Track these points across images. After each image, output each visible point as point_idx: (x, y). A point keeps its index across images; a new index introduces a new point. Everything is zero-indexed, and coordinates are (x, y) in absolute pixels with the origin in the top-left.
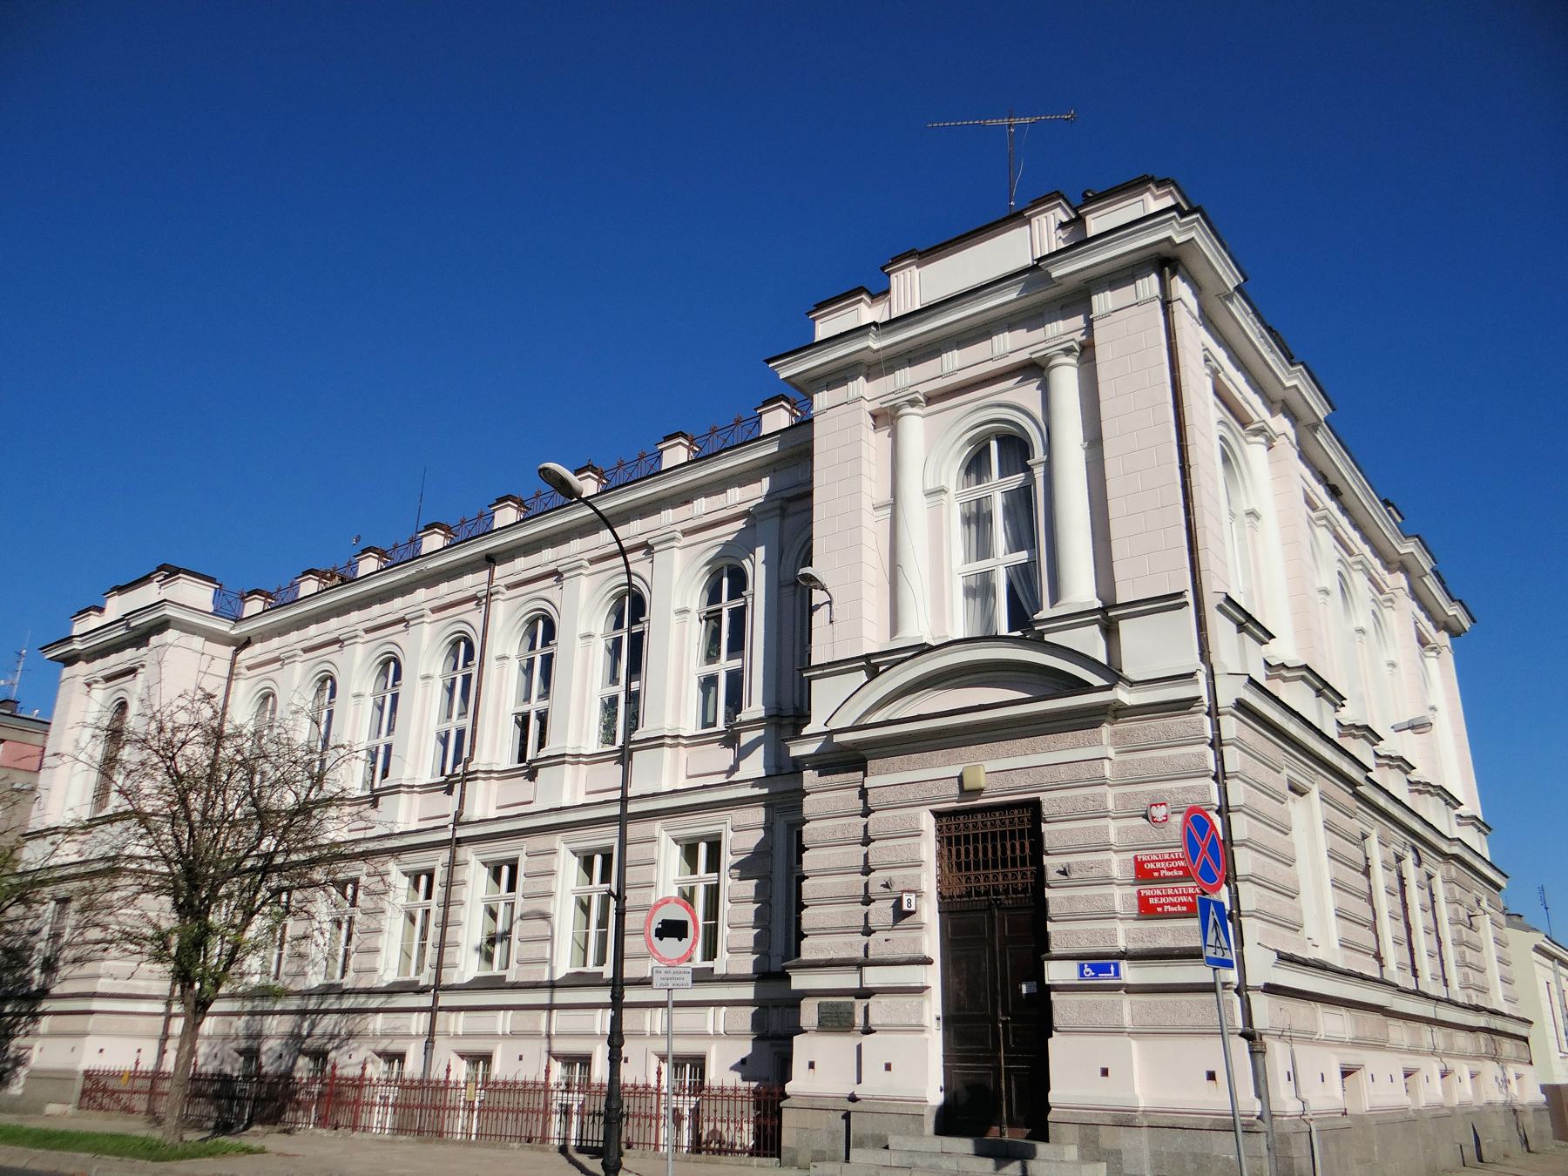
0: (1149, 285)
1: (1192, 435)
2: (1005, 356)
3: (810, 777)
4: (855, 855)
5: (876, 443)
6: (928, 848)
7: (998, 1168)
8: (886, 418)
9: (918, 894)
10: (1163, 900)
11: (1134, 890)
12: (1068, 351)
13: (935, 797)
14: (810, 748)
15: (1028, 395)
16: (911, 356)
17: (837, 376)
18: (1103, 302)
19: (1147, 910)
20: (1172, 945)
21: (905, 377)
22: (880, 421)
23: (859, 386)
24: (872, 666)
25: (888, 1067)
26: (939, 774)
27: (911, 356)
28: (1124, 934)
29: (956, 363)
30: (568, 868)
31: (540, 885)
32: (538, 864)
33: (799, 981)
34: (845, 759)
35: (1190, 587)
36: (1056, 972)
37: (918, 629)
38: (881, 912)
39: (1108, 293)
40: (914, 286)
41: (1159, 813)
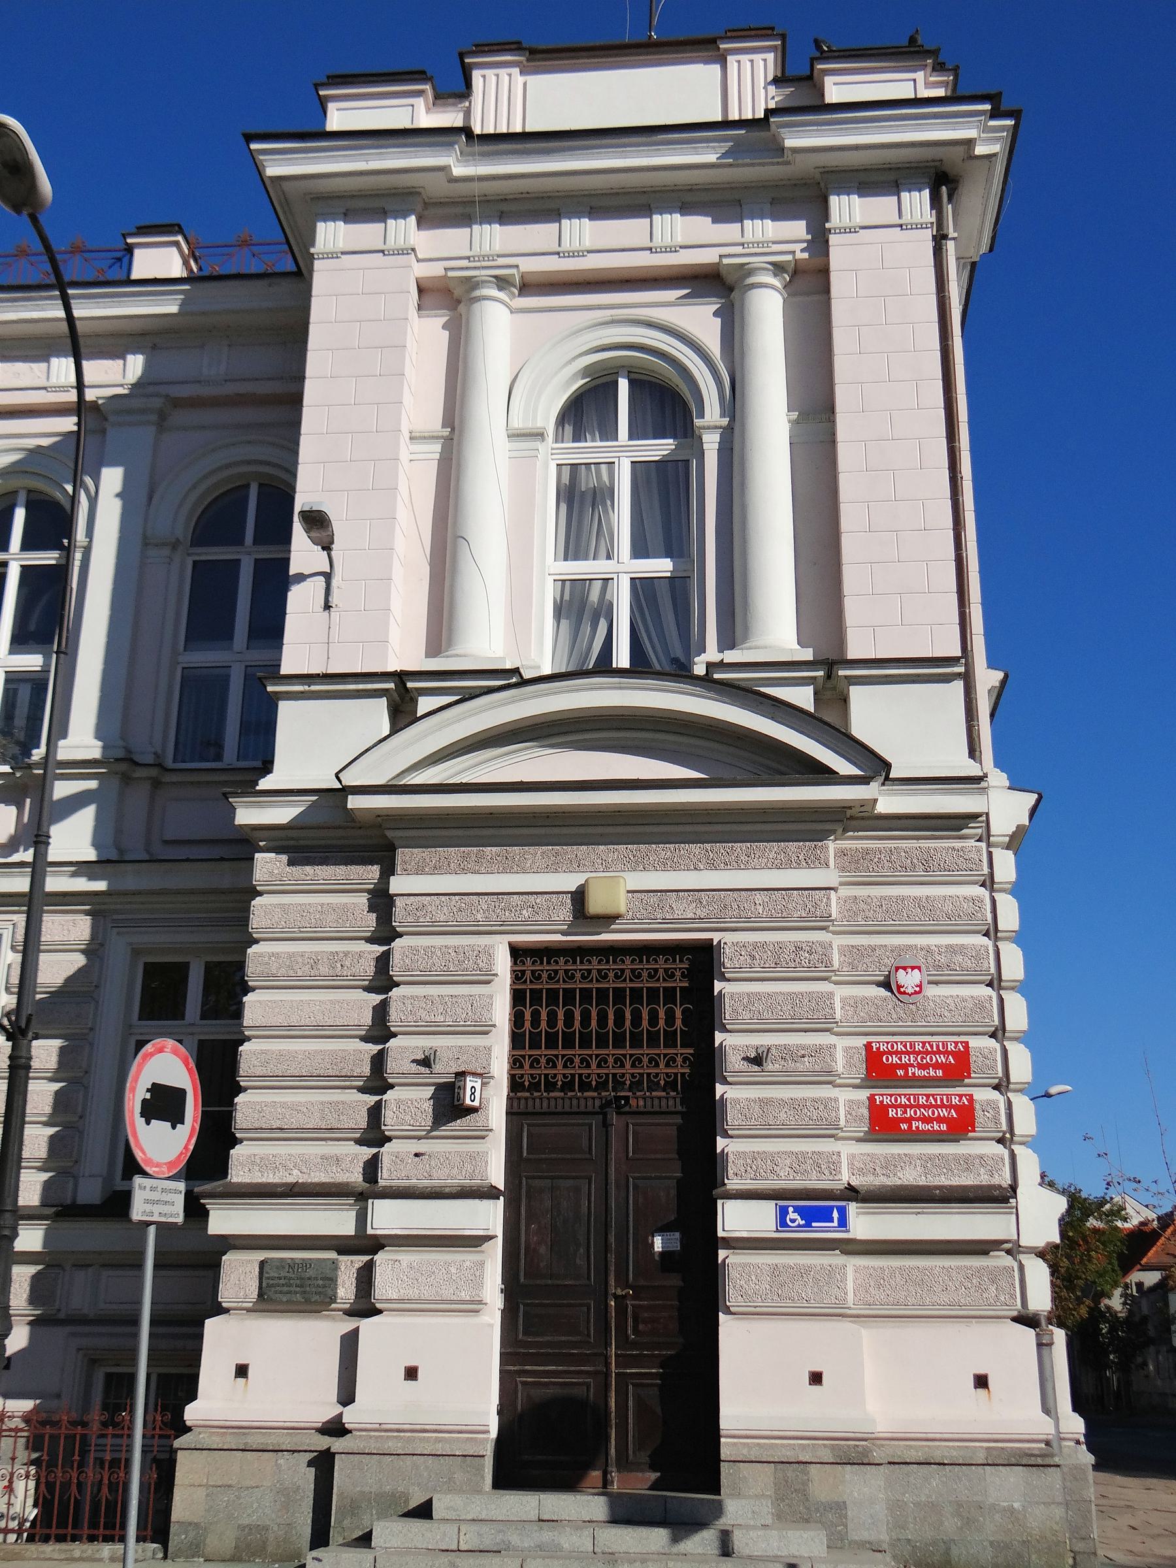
0: (917, 203)
3: (268, 865)
5: (427, 335)
7: (675, 1540)
9: (484, 1076)
10: (910, 1113)
11: (863, 1095)
12: (778, 268)
13: (525, 922)
14: (281, 814)
15: (701, 320)
16: (505, 207)
17: (370, 203)
19: (883, 1125)
20: (922, 1181)
21: (495, 239)
22: (428, 299)
23: (404, 230)
24: (401, 697)
25: (411, 1373)
26: (540, 881)
27: (505, 207)
28: (852, 1160)
29: (590, 240)
36: (736, 1218)
37: (485, 641)
38: (409, 1103)
39: (855, 198)
40: (506, 95)
41: (909, 980)
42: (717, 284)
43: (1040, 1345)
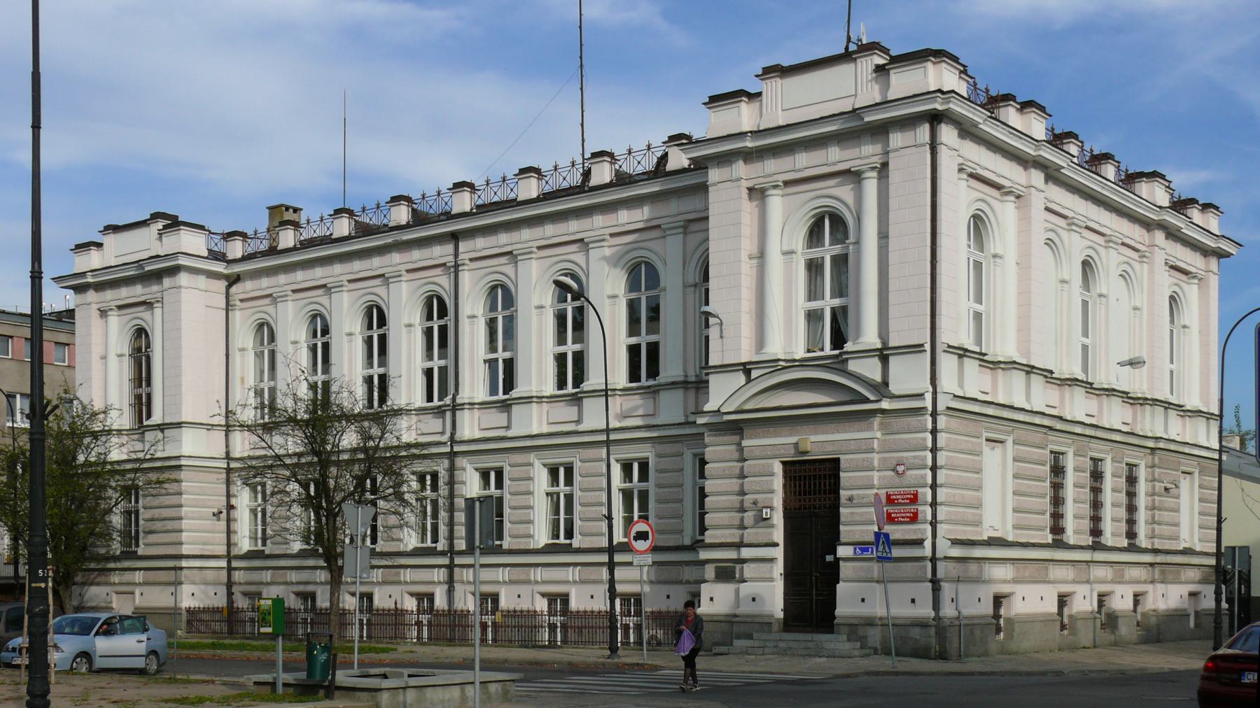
1: (943, 240)
2: (834, 164)
4: (734, 484)
5: (748, 209)
6: (778, 483)
8: (757, 193)
9: (772, 508)
15: (845, 192)
18: (897, 139)
24: (746, 368)
26: (785, 441)
29: (804, 162)
30: (541, 478)
31: (522, 486)
32: (517, 472)
33: (704, 555)
34: (735, 427)
35: (929, 341)
37: (776, 348)
38: (749, 517)
41: (900, 469)
42: (853, 176)
43: (934, 590)
